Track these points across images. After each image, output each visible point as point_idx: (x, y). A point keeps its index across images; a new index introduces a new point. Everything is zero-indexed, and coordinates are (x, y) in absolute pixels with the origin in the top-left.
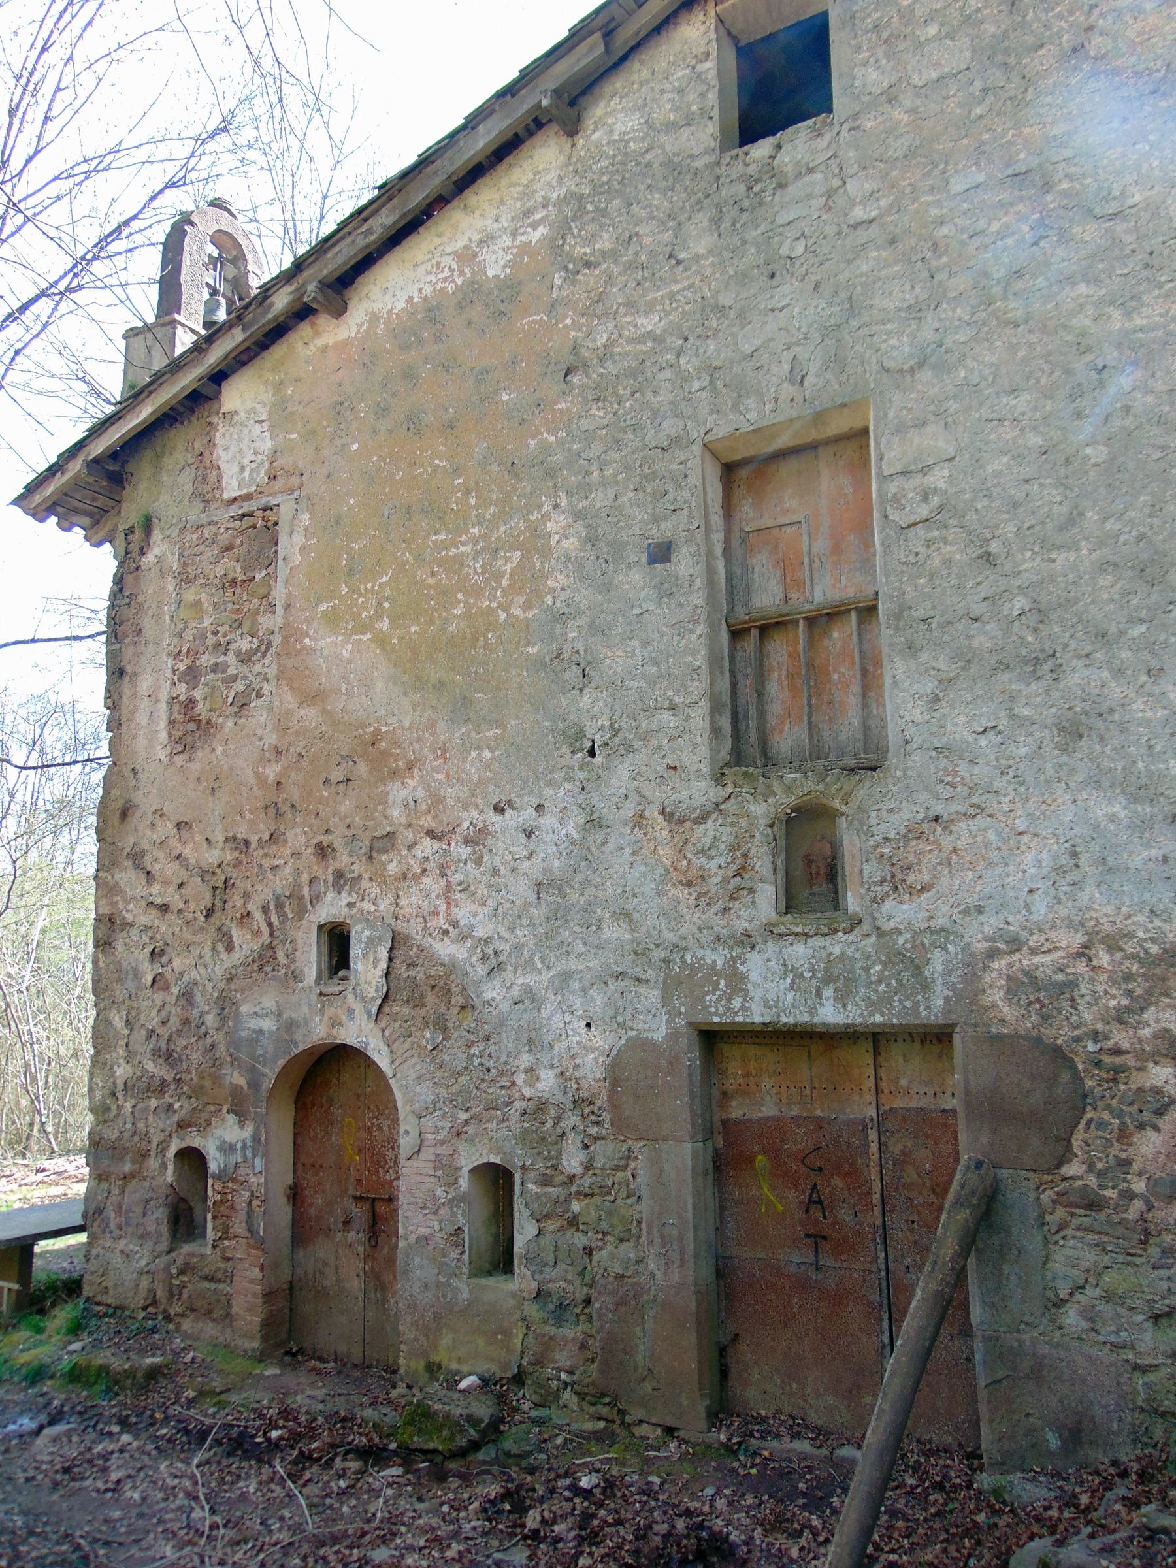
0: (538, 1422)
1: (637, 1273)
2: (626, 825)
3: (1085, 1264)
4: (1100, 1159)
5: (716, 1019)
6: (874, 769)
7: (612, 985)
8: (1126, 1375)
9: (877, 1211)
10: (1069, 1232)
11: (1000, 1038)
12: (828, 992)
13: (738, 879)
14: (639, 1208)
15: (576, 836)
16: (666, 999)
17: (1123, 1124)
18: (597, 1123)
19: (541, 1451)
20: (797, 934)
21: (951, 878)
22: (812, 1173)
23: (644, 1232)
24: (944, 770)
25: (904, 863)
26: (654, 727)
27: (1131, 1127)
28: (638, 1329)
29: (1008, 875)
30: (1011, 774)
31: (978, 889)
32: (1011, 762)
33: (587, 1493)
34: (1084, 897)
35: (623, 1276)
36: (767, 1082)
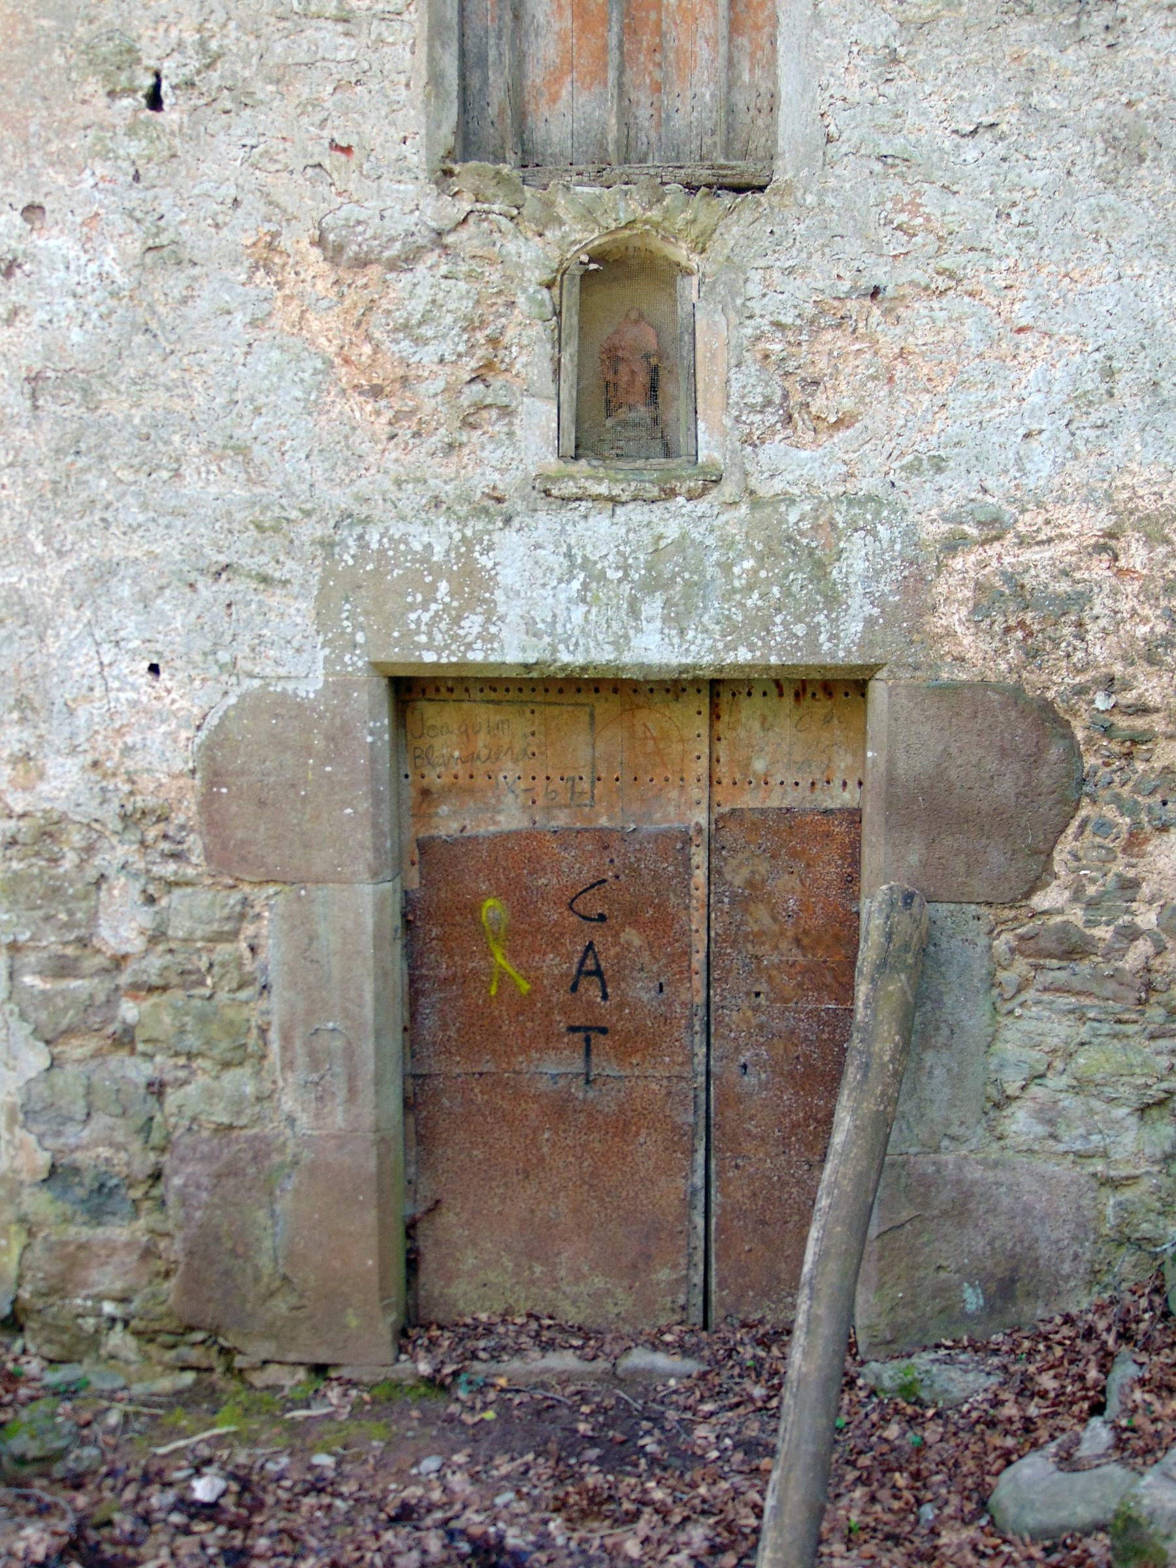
0: (67, 1392)
1: (258, 1119)
2: (236, 262)
3: (1054, 1042)
4: (1093, 881)
5: (429, 657)
6: (761, 189)
7: (206, 590)
8: (1091, 1195)
9: (699, 981)
10: (1030, 995)
11: (954, 688)
12: (653, 607)
13: (479, 387)
14: (263, 1004)
15: (121, 280)
16: (324, 617)
17: (1137, 824)
18: (175, 856)
19: (84, 1442)
20: (596, 498)
21: (892, 405)
22: (586, 925)
23: (275, 1047)
24: (896, 200)
25: (809, 373)
26: (302, 57)
27: (1148, 828)
28: (261, 1215)
29: (992, 404)
30: (1015, 218)
31: (938, 426)
32: (1017, 196)
33: (209, 1511)
34: (1116, 449)
35: (231, 1127)
36: (509, 770)
